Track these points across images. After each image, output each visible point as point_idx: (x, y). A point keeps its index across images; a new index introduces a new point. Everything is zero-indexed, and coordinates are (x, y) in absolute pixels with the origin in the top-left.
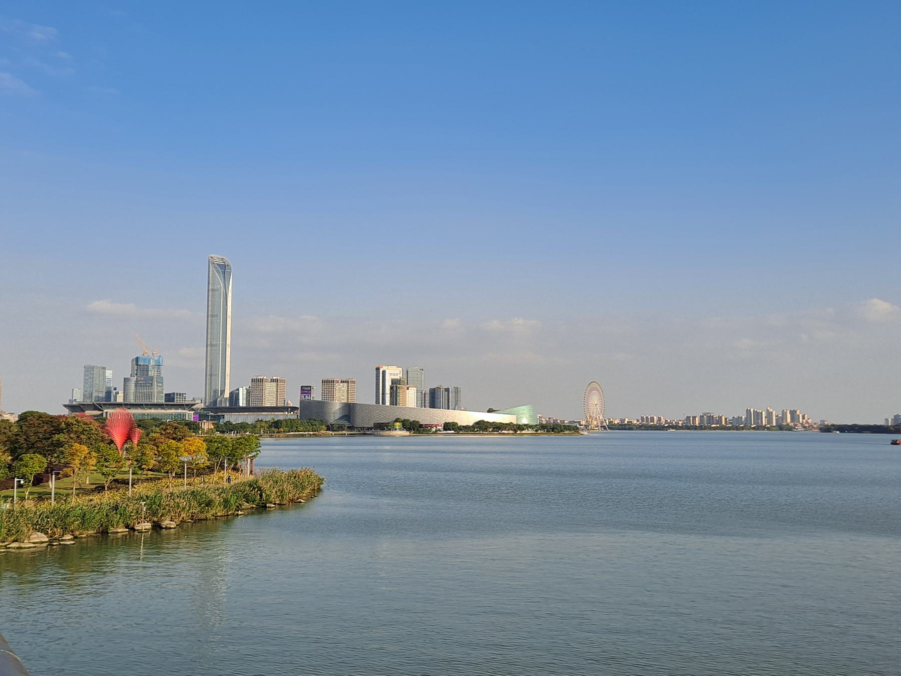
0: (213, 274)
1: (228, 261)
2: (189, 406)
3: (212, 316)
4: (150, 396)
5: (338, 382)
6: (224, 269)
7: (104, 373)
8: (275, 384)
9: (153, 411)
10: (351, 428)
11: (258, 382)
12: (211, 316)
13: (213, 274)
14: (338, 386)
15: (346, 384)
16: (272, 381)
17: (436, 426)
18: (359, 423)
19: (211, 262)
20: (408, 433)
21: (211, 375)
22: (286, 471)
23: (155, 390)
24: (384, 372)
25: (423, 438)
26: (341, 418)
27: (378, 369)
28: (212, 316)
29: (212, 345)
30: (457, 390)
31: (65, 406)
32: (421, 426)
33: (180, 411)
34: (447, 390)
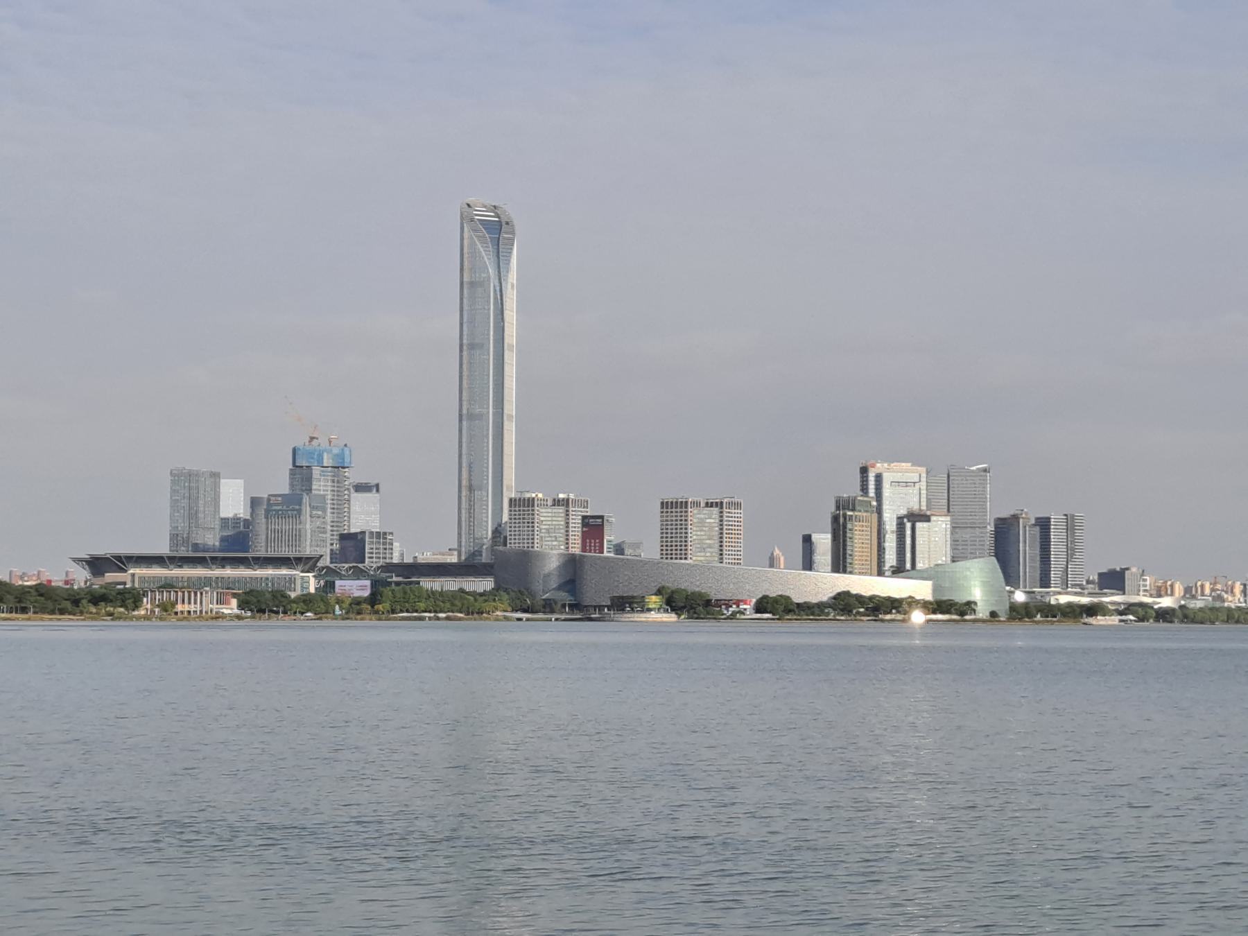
0: (472, 244)
1: (512, 211)
2: (308, 563)
3: (472, 347)
4: (297, 537)
5: (697, 504)
6: (497, 231)
7: (216, 487)
8: (561, 510)
9: (270, 572)
10: (575, 607)
11: (674, 509)
12: (469, 346)
13: (472, 244)
14: (694, 515)
15: (715, 510)
16: (557, 502)
17: (738, 603)
18: (589, 598)
19: (467, 217)
20: (671, 617)
21: (471, 488)
22: (30, 614)
23: (308, 526)
24: (879, 478)
25: (703, 633)
26: (559, 588)
27: (864, 471)
28: (472, 347)
29: (471, 417)
30: (1071, 523)
31: (77, 561)
32: (708, 603)
33: (284, 571)
34: (1044, 525)
